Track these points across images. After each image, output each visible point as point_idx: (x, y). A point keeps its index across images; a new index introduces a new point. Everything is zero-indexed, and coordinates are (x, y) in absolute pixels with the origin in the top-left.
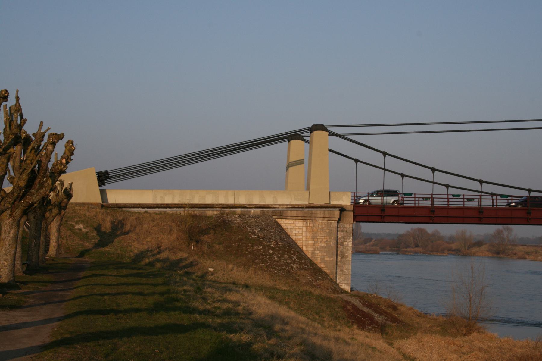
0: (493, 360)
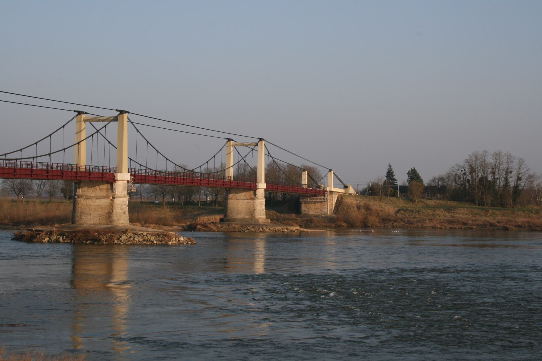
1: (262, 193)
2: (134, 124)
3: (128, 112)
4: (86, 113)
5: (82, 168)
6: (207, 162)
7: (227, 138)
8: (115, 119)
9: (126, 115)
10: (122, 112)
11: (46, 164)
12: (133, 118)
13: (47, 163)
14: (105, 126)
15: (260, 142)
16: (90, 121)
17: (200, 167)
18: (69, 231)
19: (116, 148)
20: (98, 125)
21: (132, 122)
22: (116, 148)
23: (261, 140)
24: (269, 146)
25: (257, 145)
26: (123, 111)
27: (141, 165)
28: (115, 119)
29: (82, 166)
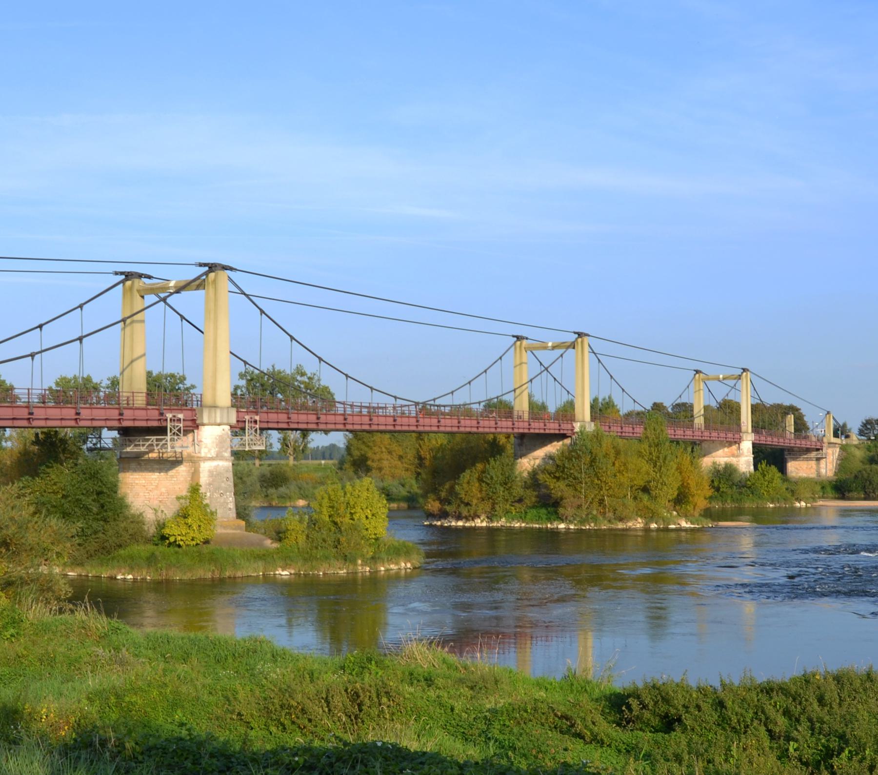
0: (876, 522)
1: (749, 448)
2: (251, 297)
3: (225, 268)
4: (527, 339)
5: (135, 398)
6: (485, 371)
7: (577, 331)
8: (573, 345)
9: (586, 339)
10: (212, 267)
11: (26, 391)
12: (598, 346)
13: (28, 389)
14: (562, 356)
15: (745, 374)
16: (531, 349)
17: (515, 390)
18: (521, 531)
19: (202, 332)
20: (547, 357)
21: (247, 293)
22: (202, 332)
23: (744, 370)
24: (757, 381)
25: (739, 377)
26: (582, 333)
27: (396, 398)
28: (573, 345)
29: (135, 394)
